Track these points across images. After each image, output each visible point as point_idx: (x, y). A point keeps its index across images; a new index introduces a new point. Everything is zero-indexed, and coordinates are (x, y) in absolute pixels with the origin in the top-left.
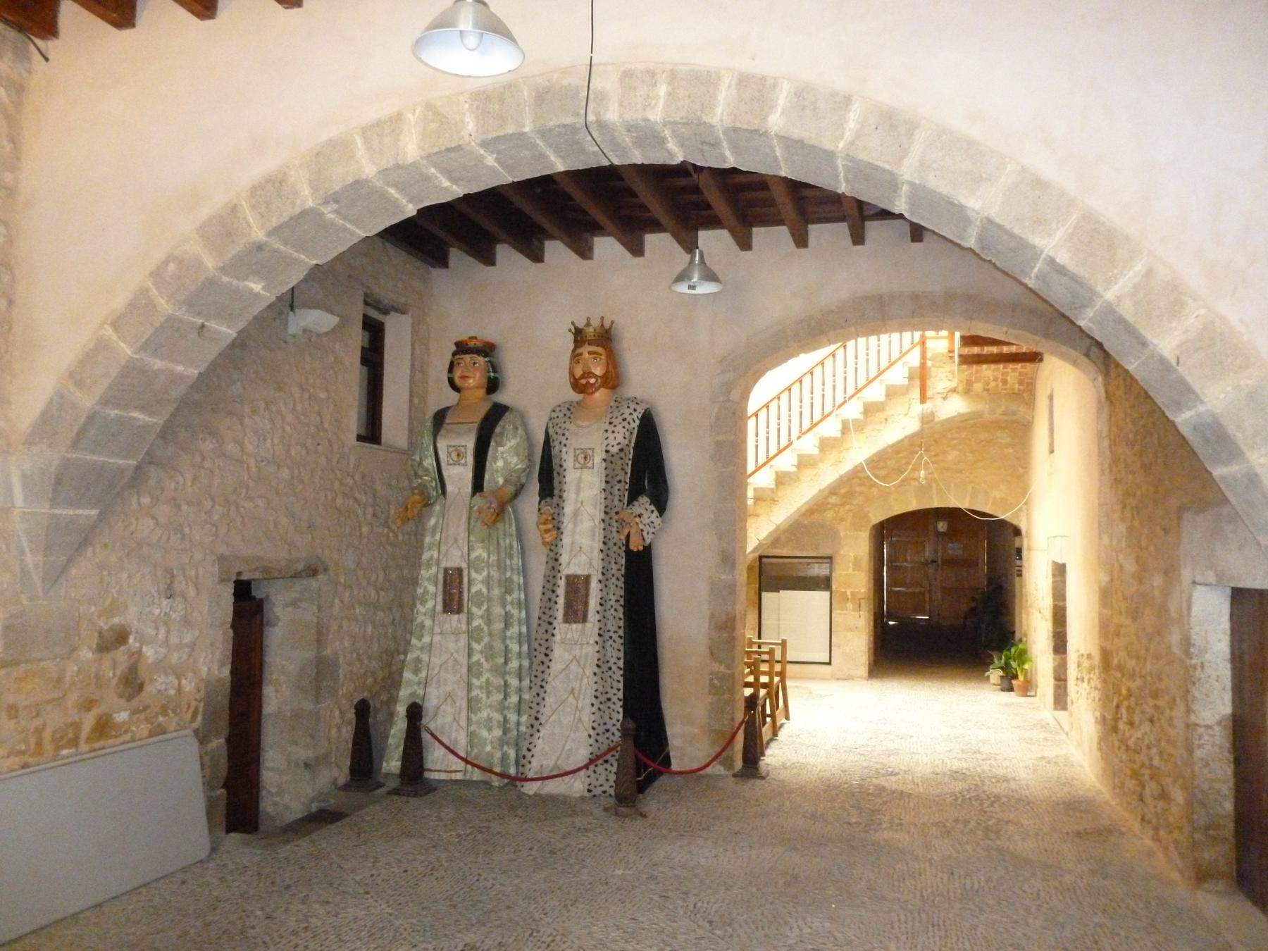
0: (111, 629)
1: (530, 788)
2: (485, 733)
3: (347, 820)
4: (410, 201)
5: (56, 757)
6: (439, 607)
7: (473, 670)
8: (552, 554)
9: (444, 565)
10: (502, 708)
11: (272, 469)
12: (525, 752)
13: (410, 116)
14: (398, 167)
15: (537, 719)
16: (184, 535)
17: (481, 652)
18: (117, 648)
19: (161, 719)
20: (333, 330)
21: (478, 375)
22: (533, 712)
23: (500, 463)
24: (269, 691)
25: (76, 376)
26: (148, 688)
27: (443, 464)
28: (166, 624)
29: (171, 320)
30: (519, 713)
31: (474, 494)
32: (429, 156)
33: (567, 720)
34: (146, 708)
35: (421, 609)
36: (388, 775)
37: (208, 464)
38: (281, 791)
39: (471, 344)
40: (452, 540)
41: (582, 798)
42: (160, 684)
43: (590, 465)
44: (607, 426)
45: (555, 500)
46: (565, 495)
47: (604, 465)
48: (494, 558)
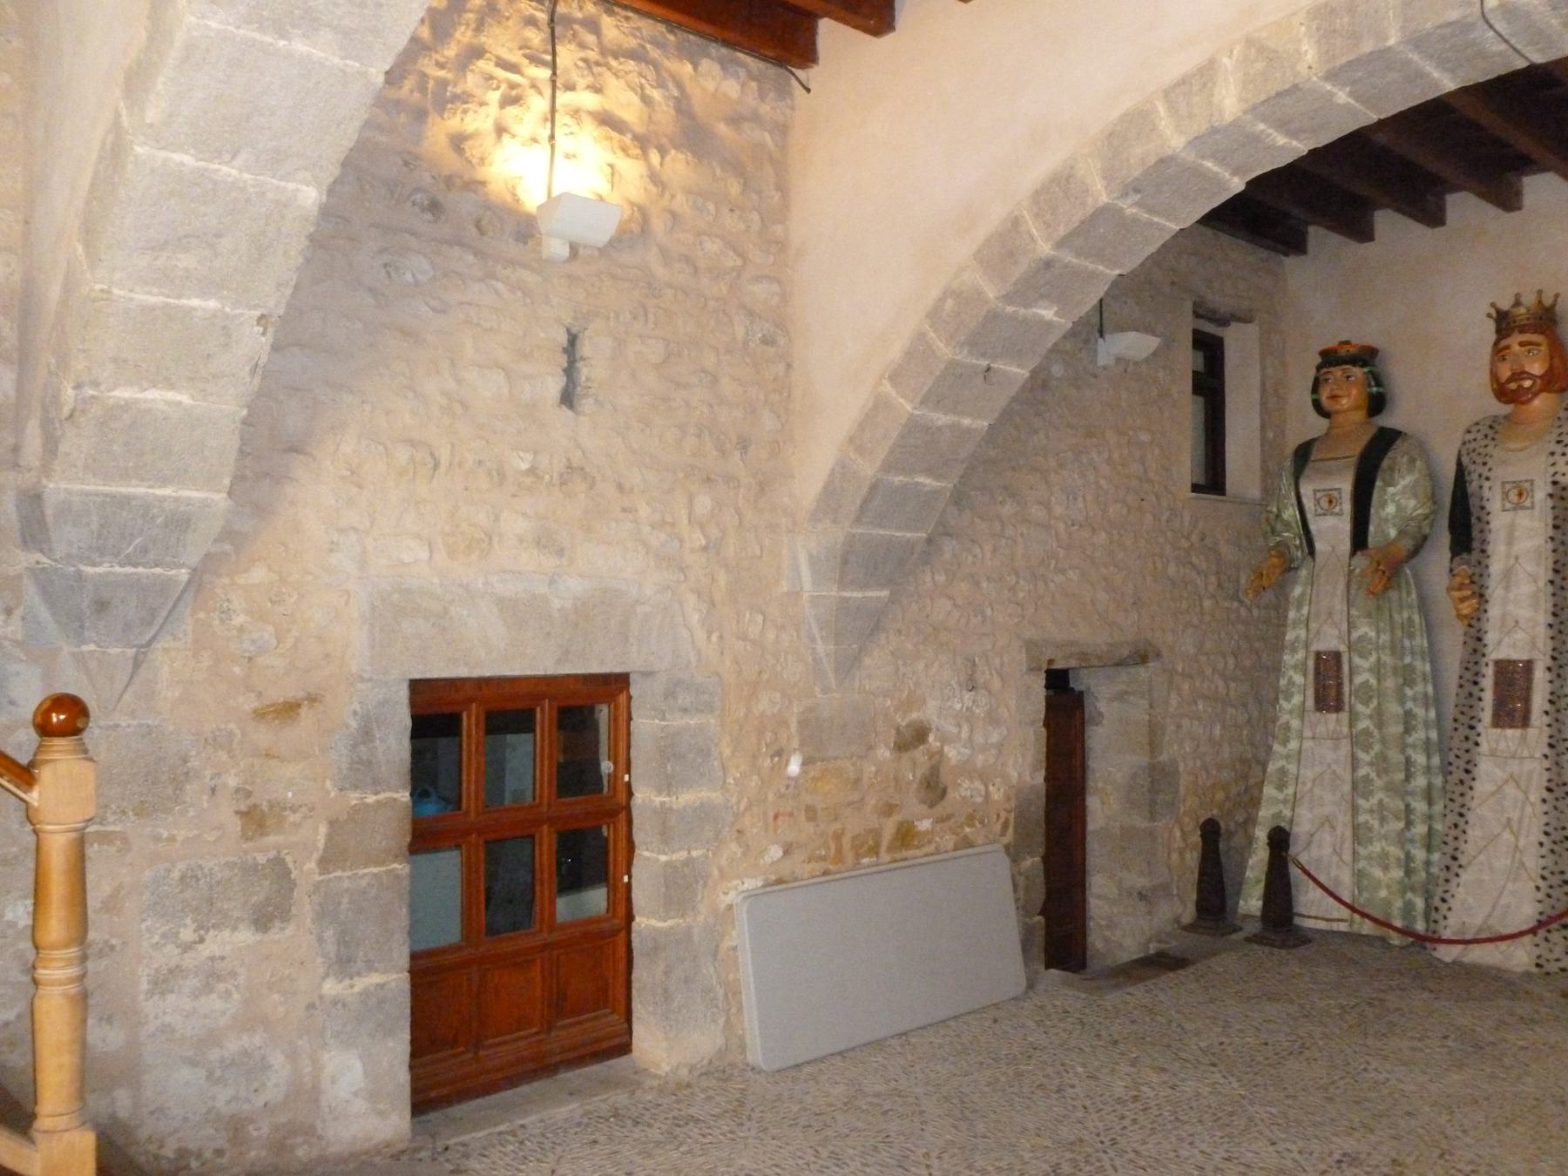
0: (909, 725)
1: (1447, 954)
2: (1378, 873)
3: (1191, 969)
4: (1235, 172)
5: (857, 865)
6: (1310, 703)
7: (1360, 787)
8: (1472, 631)
9: (1316, 647)
10: (1402, 840)
11: (1086, 534)
12: (1436, 902)
13: (1225, 60)
14: (1214, 131)
15: (1455, 858)
16: (984, 617)
17: (1371, 764)
18: (916, 747)
19: (968, 830)
20: (1155, 354)
21: (1354, 392)
22: (1449, 850)
23: (1391, 509)
24: (1093, 802)
25: (857, 442)
26: (952, 795)
27: (1309, 516)
28: (969, 721)
29: (953, 364)
30: (1429, 848)
31: (1353, 553)
32: (1254, 108)
33: (1503, 863)
34: (949, 817)
35: (1285, 705)
36: (1247, 916)
37: (1009, 532)
38: (1111, 925)
39: (1343, 352)
40: (1323, 613)
41: (1527, 974)
42: (965, 790)
43: (1528, 503)
44: (1553, 447)
45: (1475, 556)
46: (1490, 549)
47: (1550, 503)
48: (1385, 638)
